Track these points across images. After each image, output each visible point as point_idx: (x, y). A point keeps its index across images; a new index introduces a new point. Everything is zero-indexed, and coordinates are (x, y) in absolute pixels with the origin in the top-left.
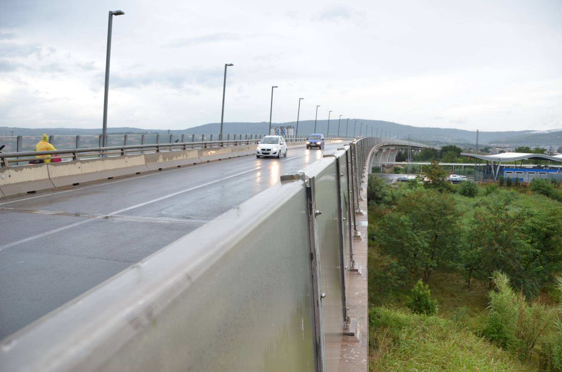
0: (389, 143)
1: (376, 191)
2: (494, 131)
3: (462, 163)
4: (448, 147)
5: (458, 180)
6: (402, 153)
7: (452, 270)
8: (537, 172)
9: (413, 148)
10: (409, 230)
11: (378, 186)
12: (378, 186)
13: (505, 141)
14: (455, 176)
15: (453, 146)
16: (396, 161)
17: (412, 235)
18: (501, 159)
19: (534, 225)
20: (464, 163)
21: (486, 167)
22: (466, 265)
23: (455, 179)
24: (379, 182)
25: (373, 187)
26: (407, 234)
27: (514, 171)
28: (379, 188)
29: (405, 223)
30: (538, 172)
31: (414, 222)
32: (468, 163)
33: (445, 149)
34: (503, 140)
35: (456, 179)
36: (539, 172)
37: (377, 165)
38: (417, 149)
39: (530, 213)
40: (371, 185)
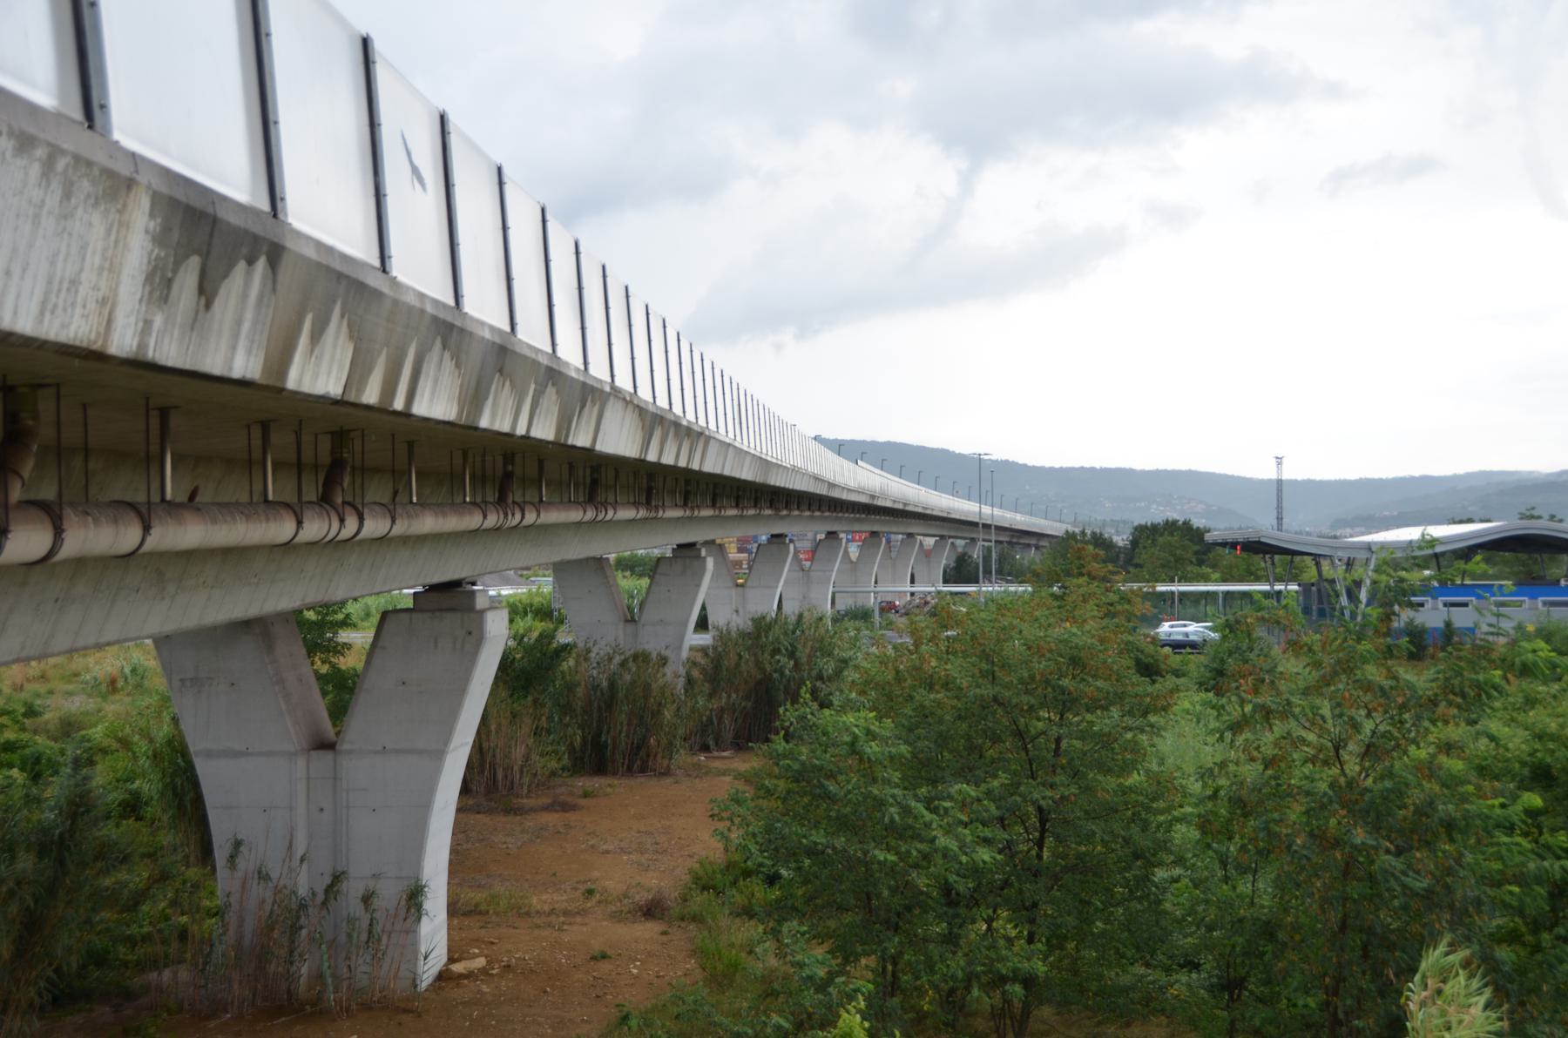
0: (905, 504)
1: (820, 677)
2: (1352, 475)
3: (1216, 581)
4: (1159, 524)
5: (1192, 638)
6: (970, 557)
7: (1150, 1004)
8: (1534, 597)
9: (1019, 537)
10: (887, 782)
11: (830, 655)
12: (830, 655)
13: (1395, 513)
14: (1185, 626)
15: (1180, 523)
16: (946, 581)
17: (906, 811)
18: (1374, 549)
19: (1538, 746)
20: (1224, 580)
21: (1314, 588)
22: (1215, 980)
23: (1180, 638)
24: (832, 638)
25: (804, 660)
26: (880, 804)
27: (1435, 598)
28: (831, 665)
29: (868, 750)
30: (1536, 598)
31: (919, 744)
32: (1241, 580)
33: (1146, 534)
34: (1387, 513)
35: (1187, 635)
36: (1540, 599)
37: (860, 603)
38: (1033, 541)
39: (1517, 660)
40: (798, 654)
